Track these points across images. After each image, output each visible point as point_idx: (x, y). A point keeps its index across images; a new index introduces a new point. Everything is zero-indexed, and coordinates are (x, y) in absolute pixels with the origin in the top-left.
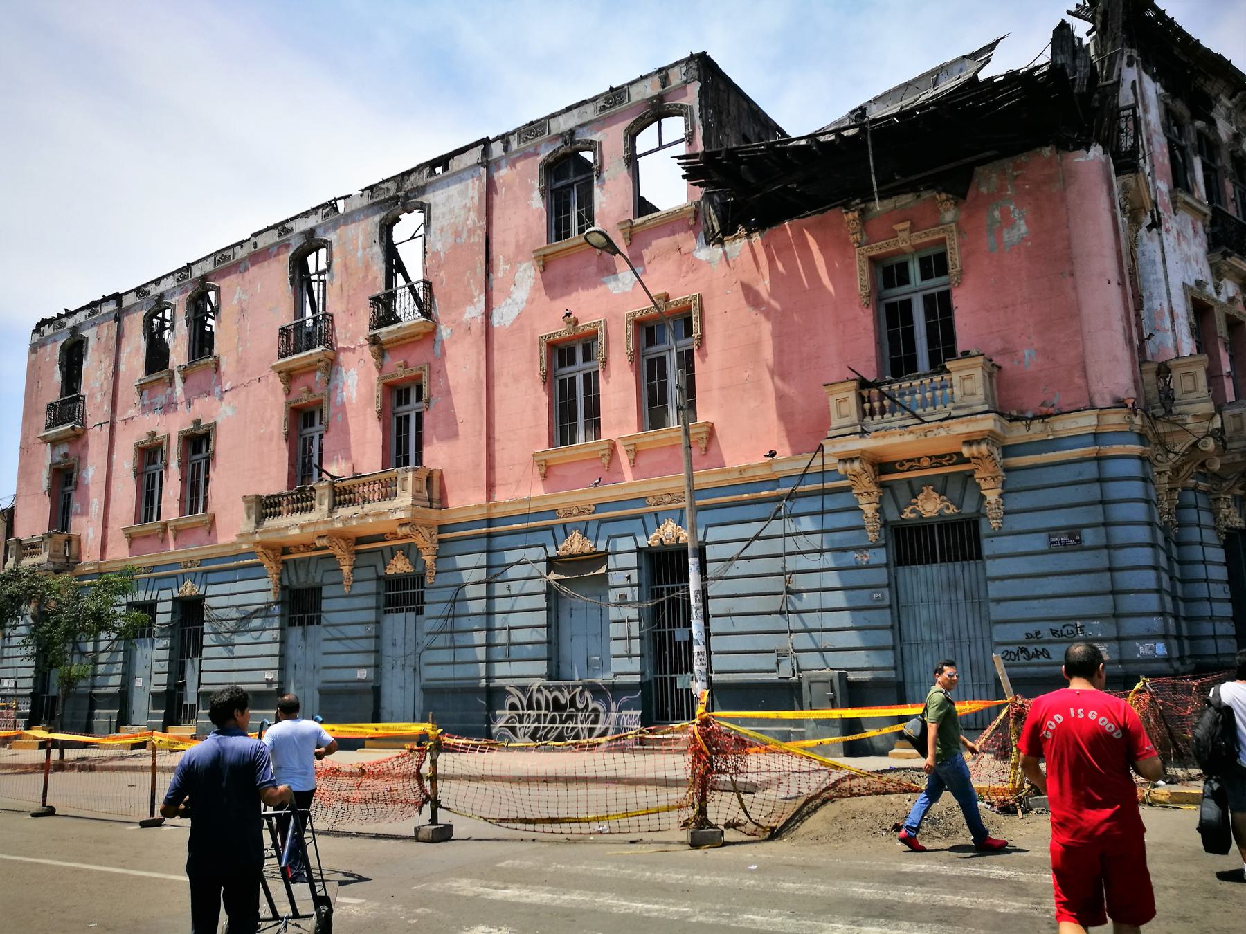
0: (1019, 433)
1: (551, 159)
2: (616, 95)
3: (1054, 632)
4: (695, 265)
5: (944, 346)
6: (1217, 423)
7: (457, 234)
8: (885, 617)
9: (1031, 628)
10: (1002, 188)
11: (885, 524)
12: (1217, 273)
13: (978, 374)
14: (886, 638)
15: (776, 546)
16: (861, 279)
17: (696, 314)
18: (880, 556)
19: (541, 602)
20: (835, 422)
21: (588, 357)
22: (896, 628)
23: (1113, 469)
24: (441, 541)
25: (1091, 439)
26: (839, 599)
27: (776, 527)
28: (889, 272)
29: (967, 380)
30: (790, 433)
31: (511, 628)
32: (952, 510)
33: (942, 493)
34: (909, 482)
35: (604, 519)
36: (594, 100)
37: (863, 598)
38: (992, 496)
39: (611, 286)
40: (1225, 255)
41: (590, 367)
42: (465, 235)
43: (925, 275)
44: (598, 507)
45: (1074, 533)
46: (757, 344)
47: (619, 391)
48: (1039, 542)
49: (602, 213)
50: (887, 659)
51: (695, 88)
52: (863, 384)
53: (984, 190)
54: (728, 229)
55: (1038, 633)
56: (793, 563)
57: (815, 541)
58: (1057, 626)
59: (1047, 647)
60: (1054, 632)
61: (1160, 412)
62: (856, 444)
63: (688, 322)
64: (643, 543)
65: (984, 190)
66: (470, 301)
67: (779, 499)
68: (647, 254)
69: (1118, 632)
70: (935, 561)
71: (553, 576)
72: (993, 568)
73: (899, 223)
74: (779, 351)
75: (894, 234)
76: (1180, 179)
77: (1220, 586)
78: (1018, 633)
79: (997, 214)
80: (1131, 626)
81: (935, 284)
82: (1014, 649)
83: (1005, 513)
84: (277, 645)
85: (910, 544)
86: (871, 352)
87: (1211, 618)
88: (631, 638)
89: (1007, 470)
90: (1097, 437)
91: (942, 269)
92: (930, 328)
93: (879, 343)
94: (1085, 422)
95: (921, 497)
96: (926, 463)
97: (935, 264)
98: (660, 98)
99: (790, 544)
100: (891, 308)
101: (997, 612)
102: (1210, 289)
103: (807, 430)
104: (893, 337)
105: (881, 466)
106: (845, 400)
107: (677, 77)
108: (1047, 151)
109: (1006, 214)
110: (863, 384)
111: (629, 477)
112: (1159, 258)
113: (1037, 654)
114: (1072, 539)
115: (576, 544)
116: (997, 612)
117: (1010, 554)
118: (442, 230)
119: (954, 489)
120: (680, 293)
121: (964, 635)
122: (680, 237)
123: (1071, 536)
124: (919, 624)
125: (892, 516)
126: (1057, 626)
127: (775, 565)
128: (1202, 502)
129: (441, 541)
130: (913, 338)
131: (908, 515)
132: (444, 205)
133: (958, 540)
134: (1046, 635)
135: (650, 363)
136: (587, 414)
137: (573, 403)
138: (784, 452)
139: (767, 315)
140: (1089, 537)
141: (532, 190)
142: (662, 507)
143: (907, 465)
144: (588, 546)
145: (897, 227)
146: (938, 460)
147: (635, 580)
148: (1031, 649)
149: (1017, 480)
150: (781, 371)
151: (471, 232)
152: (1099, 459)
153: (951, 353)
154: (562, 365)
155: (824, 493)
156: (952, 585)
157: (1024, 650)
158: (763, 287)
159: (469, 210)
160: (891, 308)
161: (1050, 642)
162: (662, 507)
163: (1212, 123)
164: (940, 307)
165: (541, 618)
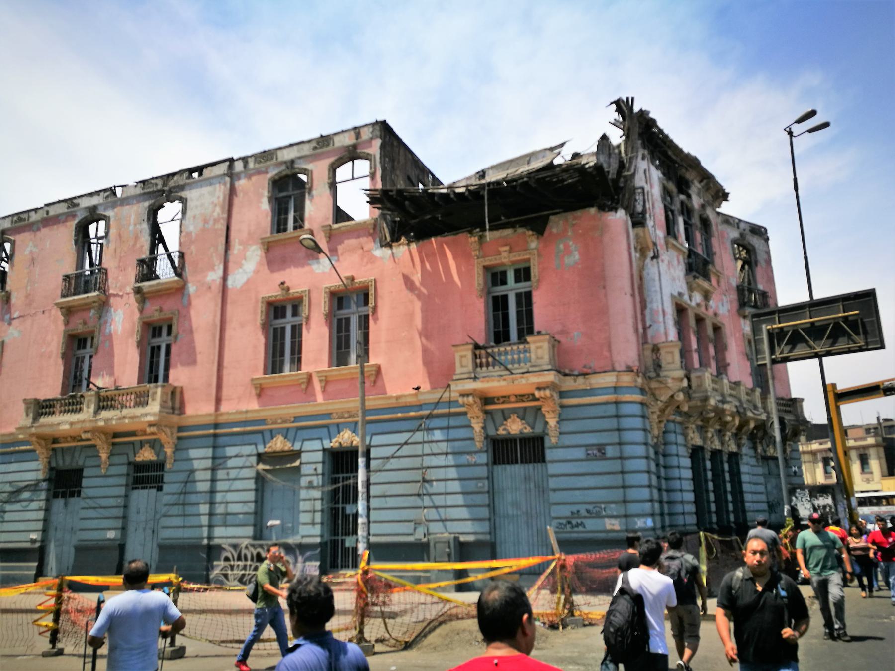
2: (324, 141)
3: (588, 511)
4: (373, 260)
5: (527, 328)
7: (206, 221)
8: (484, 499)
9: (575, 508)
10: (565, 231)
12: (691, 289)
13: (546, 345)
15: (418, 449)
16: (478, 279)
17: (372, 291)
18: (483, 458)
19: (251, 484)
20: (459, 370)
21: (295, 313)
22: (492, 506)
24: (179, 438)
25: (612, 390)
27: (419, 436)
28: (497, 277)
29: (539, 349)
30: (430, 374)
32: (528, 430)
33: (522, 419)
34: (503, 411)
35: (300, 428)
36: (309, 141)
37: (471, 485)
38: (552, 422)
40: (695, 277)
42: (211, 223)
43: (517, 280)
44: (297, 419)
45: (601, 448)
46: (411, 315)
48: (580, 453)
50: (485, 527)
52: (477, 347)
53: (554, 230)
54: (395, 238)
55: (578, 512)
56: (428, 461)
58: (590, 507)
59: (584, 521)
60: (588, 511)
61: (653, 374)
62: (471, 385)
63: (367, 296)
65: (554, 230)
66: (212, 268)
67: (421, 418)
68: (340, 248)
69: (626, 511)
70: (516, 462)
71: (261, 467)
72: (552, 469)
73: (504, 246)
74: (425, 320)
75: (499, 253)
76: (670, 230)
77: (688, 482)
78: (566, 511)
79: (562, 246)
80: (633, 508)
81: (523, 287)
82: (564, 521)
85: (503, 451)
86: (482, 326)
87: (682, 502)
89: (562, 406)
90: (616, 389)
92: (519, 313)
93: (487, 321)
94: (608, 380)
95: (509, 420)
96: (513, 399)
97: (523, 274)
98: (354, 147)
99: (427, 449)
100: (495, 299)
101: (555, 497)
102: (686, 297)
103: (441, 373)
105: (486, 400)
106: (465, 356)
107: (366, 134)
109: (567, 246)
110: (477, 347)
111: (320, 398)
112: (657, 278)
113: (577, 525)
115: (279, 444)
116: (555, 497)
120: (362, 277)
121: (533, 512)
122: (363, 240)
123: (599, 451)
124: (505, 504)
125: (492, 432)
126: (590, 507)
127: (416, 462)
128: (679, 429)
130: (508, 319)
131: (501, 432)
133: (532, 449)
134: (583, 513)
135: (339, 321)
136: (293, 353)
138: (426, 387)
139: (419, 296)
140: (610, 451)
141: (261, 196)
142: (342, 420)
143: (501, 400)
144: (288, 446)
146: (521, 397)
148: (574, 522)
149: (571, 413)
150: (425, 333)
151: (216, 221)
152: (617, 403)
153: (530, 331)
154: (276, 317)
155: (450, 415)
156: (527, 479)
157: (569, 523)
158: (417, 278)
159: (216, 205)
160: (495, 299)
161: (585, 517)
162: (342, 420)
163: (689, 196)
164: (525, 300)
165: (251, 496)
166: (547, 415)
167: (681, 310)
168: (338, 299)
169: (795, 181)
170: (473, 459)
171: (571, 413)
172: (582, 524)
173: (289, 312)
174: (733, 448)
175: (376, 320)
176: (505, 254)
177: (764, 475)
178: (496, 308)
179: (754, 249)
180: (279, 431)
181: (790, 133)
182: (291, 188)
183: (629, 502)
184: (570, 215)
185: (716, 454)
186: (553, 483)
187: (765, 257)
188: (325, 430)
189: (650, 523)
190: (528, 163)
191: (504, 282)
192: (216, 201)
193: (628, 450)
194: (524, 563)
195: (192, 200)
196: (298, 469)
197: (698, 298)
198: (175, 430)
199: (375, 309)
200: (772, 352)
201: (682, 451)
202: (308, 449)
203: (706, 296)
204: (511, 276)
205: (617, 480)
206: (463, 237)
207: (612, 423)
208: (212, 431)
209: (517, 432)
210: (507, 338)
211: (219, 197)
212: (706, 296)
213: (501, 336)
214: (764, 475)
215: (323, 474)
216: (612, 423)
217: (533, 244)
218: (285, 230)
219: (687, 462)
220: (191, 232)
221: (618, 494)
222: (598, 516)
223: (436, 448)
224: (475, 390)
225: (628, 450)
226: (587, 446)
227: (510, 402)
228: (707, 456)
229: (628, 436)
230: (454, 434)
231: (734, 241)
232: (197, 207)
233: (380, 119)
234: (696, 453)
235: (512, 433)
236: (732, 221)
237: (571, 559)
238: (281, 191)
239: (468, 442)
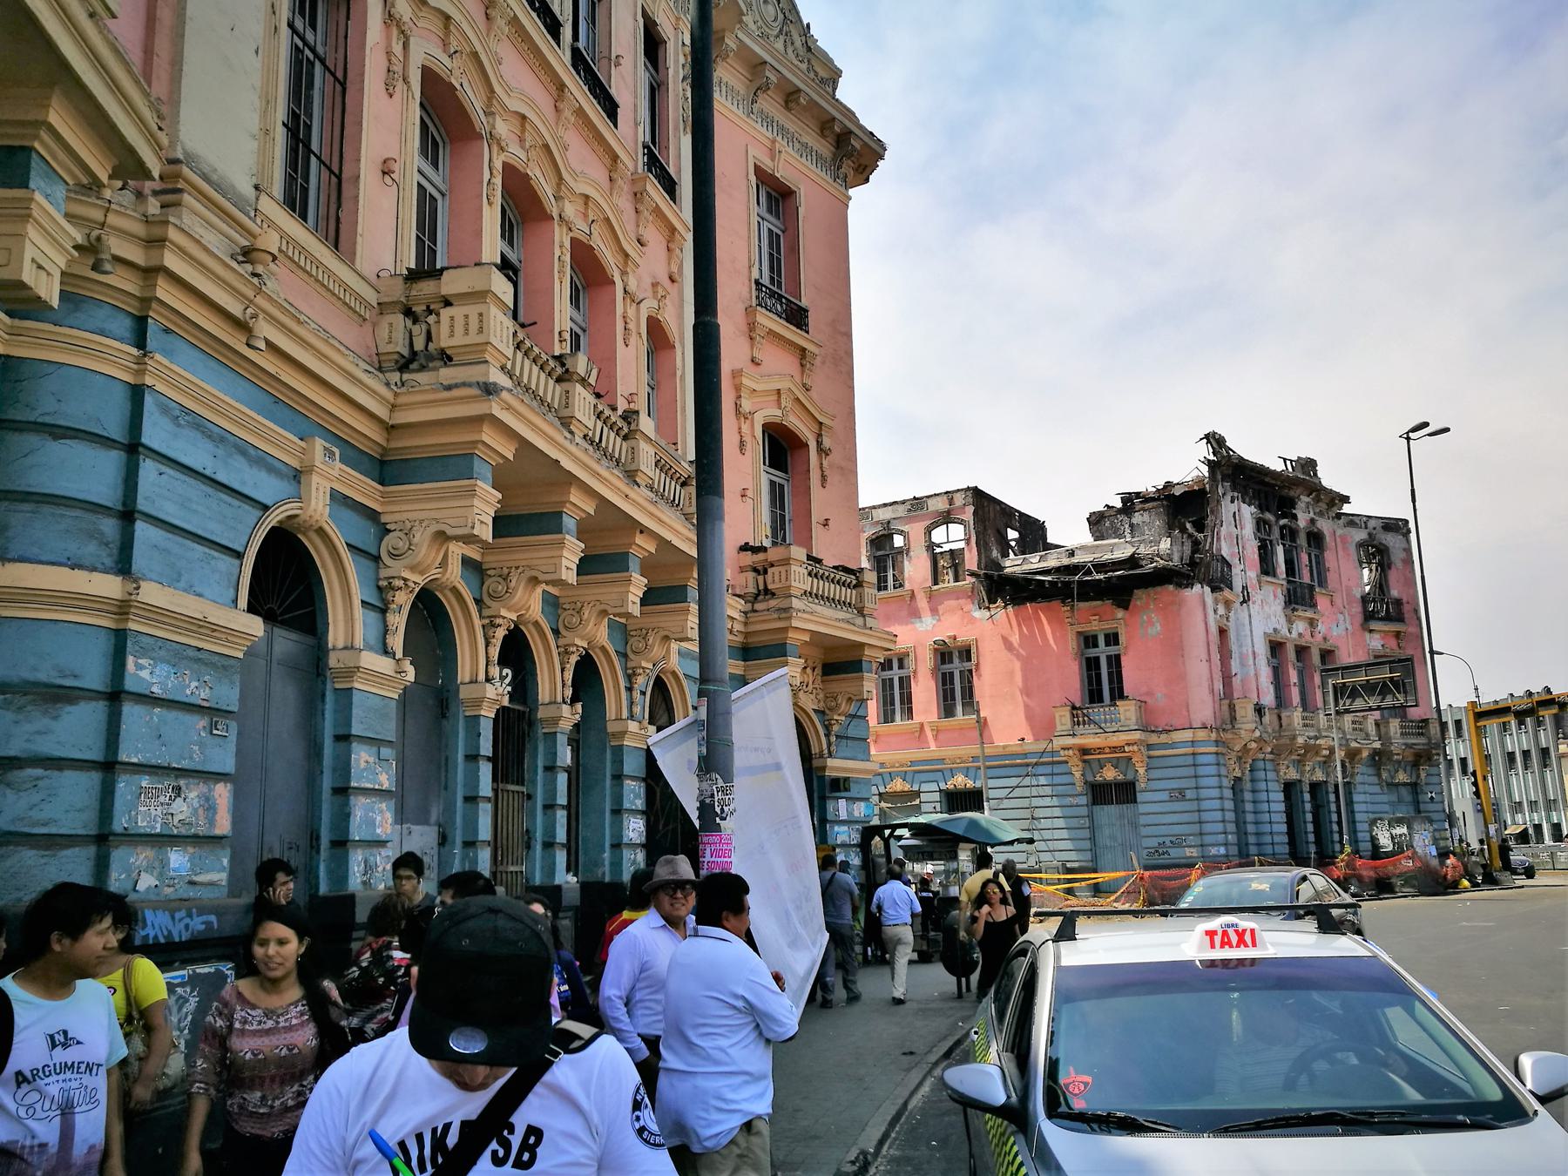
0: (1154, 739)
2: (917, 503)
4: (973, 620)
5: (1118, 693)
6: (1257, 734)
8: (1086, 834)
9: (1161, 840)
10: (1148, 604)
12: (1290, 621)
13: (1133, 708)
14: (1087, 844)
15: (1026, 792)
16: (1072, 643)
17: (973, 650)
18: (1083, 800)
20: (1059, 728)
21: (901, 667)
22: (1093, 839)
23: (1201, 759)
26: (1061, 823)
27: (1027, 781)
28: (1089, 641)
29: (1127, 711)
30: (1032, 728)
35: (916, 771)
36: (903, 502)
37: (1074, 823)
38: (1141, 771)
39: (918, 625)
40: (1294, 610)
41: (903, 673)
43: (1107, 644)
44: (913, 763)
45: (1182, 792)
46: (1012, 673)
47: (925, 692)
48: (1164, 796)
50: (1088, 855)
51: (971, 509)
52: (1074, 708)
54: (992, 601)
56: (1036, 802)
57: (1048, 790)
62: (1070, 741)
63: (968, 652)
64: (943, 787)
68: (941, 608)
71: (883, 804)
72: (1142, 808)
73: (1097, 617)
74: (1025, 679)
76: (1267, 568)
78: (1154, 842)
80: (1208, 839)
81: (1112, 650)
85: (1101, 794)
86: (1078, 686)
91: (1116, 643)
92: (1110, 674)
94: (1187, 735)
97: (1113, 639)
98: (949, 512)
99: (1035, 791)
100: (1088, 660)
101: (1144, 831)
102: (1285, 631)
103: (1044, 728)
104: (1090, 677)
105: (1084, 751)
107: (959, 500)
109: (1150, 618)
110: (1074, 708)
111: (933, 748)
114: (1180, 795)
115: (898, 785)
116: (1144, 831)
117: (1151, 801)
119: (1122, 765)
120: (964, 636)
122: (962, 601)
124: (1104, 837)
125: (1090, 778)
127: (1025, 803)
128: (1269, 766)
130: (1101, 682)
133: (1125, 792)
135: (944, 675)
136: (902, 702)
137: (892, 695)
138: (1029, 739)
139: (1018, 656)
140: (1189, 794)
144: (907, 787)
146: (1114, 749)
149: (1155, 763)
150: (1027, 691)
153: (1122, 696)
155: (1053, 763)
156: (1122, 817)
158: (1015, 639)
160: (1088, 660)
163: (1295, 517)
164: (1115, 662)
167: (1276, 647)
168: (944, 654)
169: (1413, 491)
171: (1155, 763)
173: (895, 665)
175: (979, 676)
177: (1390, 803)
178: (1089, 668)
179: (1387, 549)
180: (898, 774)
181: (1408, 439)
184: (1151, 590)
185: (1315, 787)
186: (1143, 820)
187: (1403, 555)
189: (1222, 850)
191: (1096, 645)
193: (1204, 793)
194: (1118, 874)
196: (918, 807)
197: (1300, 626)
199: (977, 665)
200: (1337, 704)
201: (1273, 786)
203: (1312, 623)
205: (1195, 817)
206: (1056, 604)
207: (1190, 771)
210: (1101, 700)
212: (1312, 623)
213: (1095, 696)
214: (1390, 803)
216: (1190, 771)
217: (1120, 613)
218: (886, 588)
219: (1281, 796)
221: (1196, 828)
222: (1180, 846)
223: (1042, 791)
225: (1204, 793)
228: (1306, 788)
229: (1204, 782)
230: (1057, 780)
231: (1360, 545)
233: (972, 485)
234: (1289, 788)
236: (1356, 520)
237: (1147, 874)
238: (879, 549)
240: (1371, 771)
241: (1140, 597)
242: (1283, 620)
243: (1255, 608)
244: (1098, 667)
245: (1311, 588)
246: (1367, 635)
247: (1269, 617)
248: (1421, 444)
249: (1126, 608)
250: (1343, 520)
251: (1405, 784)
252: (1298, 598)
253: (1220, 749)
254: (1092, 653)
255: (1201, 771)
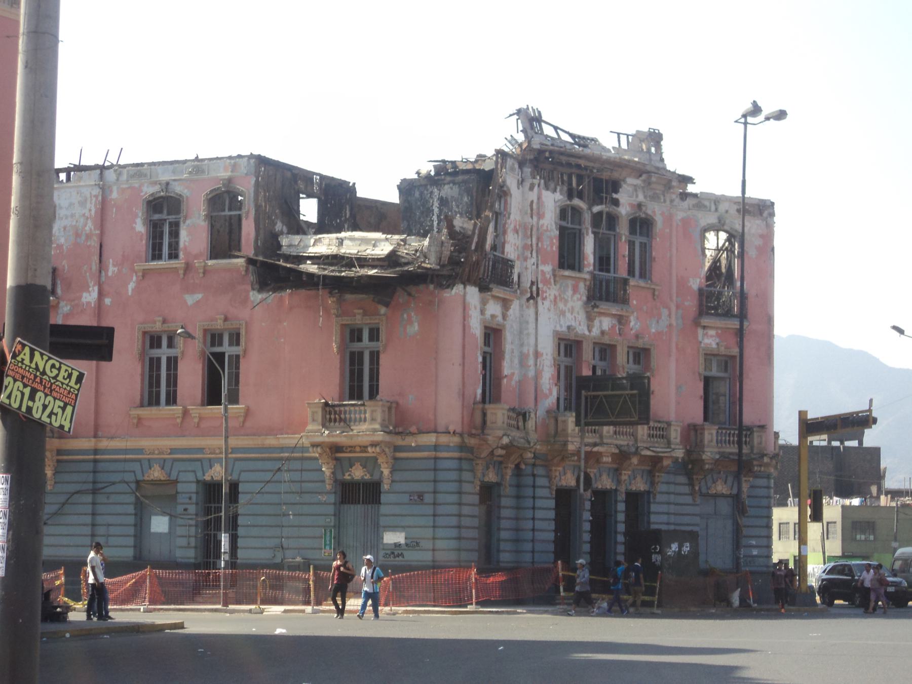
0: (399, 441)
1: (151, 198)
7: (77, 235)
11: (336, 481)
12: (590, 319)
18: (332, 498)
19: (131, 509)
21: (170, 345)
24: (58, 461)
28: (355, 334)
31: (109, 525)
32: (367, 477)
33: (364, 467)
34: (350, 458)
38: (386, 472)
40: (595, 306)
41: (172, 352)
42: (83, 238)
44: (173, 451)
45: (421, 496)
49: (185, 247)
65: (401, 300)
66: (86, 288)
67: (281, 459)
70: (359, 503)
72: (384, 509)
76: (568, 258)
79: (405, 316)
82: (389, 552)
83: (393, 481)
84: (381, 524)
88: (190, 536)
89: (395, 459)
90: (436, 448)
93: (342, 375)
94: (430, 439)
96: (358, 449)
97: (374, 335)
100: (352, 354)
104: (352, 373)
105: (336, 449)
106: (316, 412)
108: (431, 287)
109: (409, 317)
113: (398, 556)
118: (65, 228)
123: (419, 497)
125: (339, 477)
129: (58, 461)
131: (347, 477)
132: (67, 209)
140: (428, 498)
141: (136, 216)
142: (213, 456)
143: (349, 449)
145: (356, 311)
147: (193, 544)
148: (396, 553)
151: (89, 237)
152: (436, 458)
154: (152, 347)
157: (393, 553)
159: (87, 218)
162: (213, 456)
163: (616, 203)
164: (375, 357)
165: (131, 520)
166: (382, 466)
170: (323, 498)
172: (402, 555)
173: (164, 342)
174: (640, 485)
176: (358, 317)
178: (352, 363)
181: (746, 124)
182: (165, 211)
183: (455, 539)
185: (602, 498)
187: (758, 242)
188: (199, 463)
190: (374, 246)
191: (360, 340)
192: (86, 212)
195: (61, 208)
198: (55, 453)
199: (245, 351)
202: (184, 480)
203: (621, 320)
204: (366, 335)
207: (430, 475)
208: (92, 457)
209: (359, 478)
211: (90, 210)
212: (621, 320)
215: (197, 504)
217: (383, 310)
220: (62, 245)
224: (323, 443)
226: (411, 494)
227: (355, 452)
228: (622, 497)
232: (67, 217)
233: (256, 153)
234: (564, 498)
235: (356, 478)
236: (707, 203)
239: (320, 484)
240: (683, 479)
241: (400, 297)
242: (582, 316)
243: (544, 306)
244: (361, 363)
245: (625, 282)
246: (700, 332)
247: (563, 313)
248: (759, 130)
249: (387, 305)
250: (690, 201)
251: (723, 496)
252: (604, 292)
253: (463, 455)
254: (356, 347)
255: (441, 475)
